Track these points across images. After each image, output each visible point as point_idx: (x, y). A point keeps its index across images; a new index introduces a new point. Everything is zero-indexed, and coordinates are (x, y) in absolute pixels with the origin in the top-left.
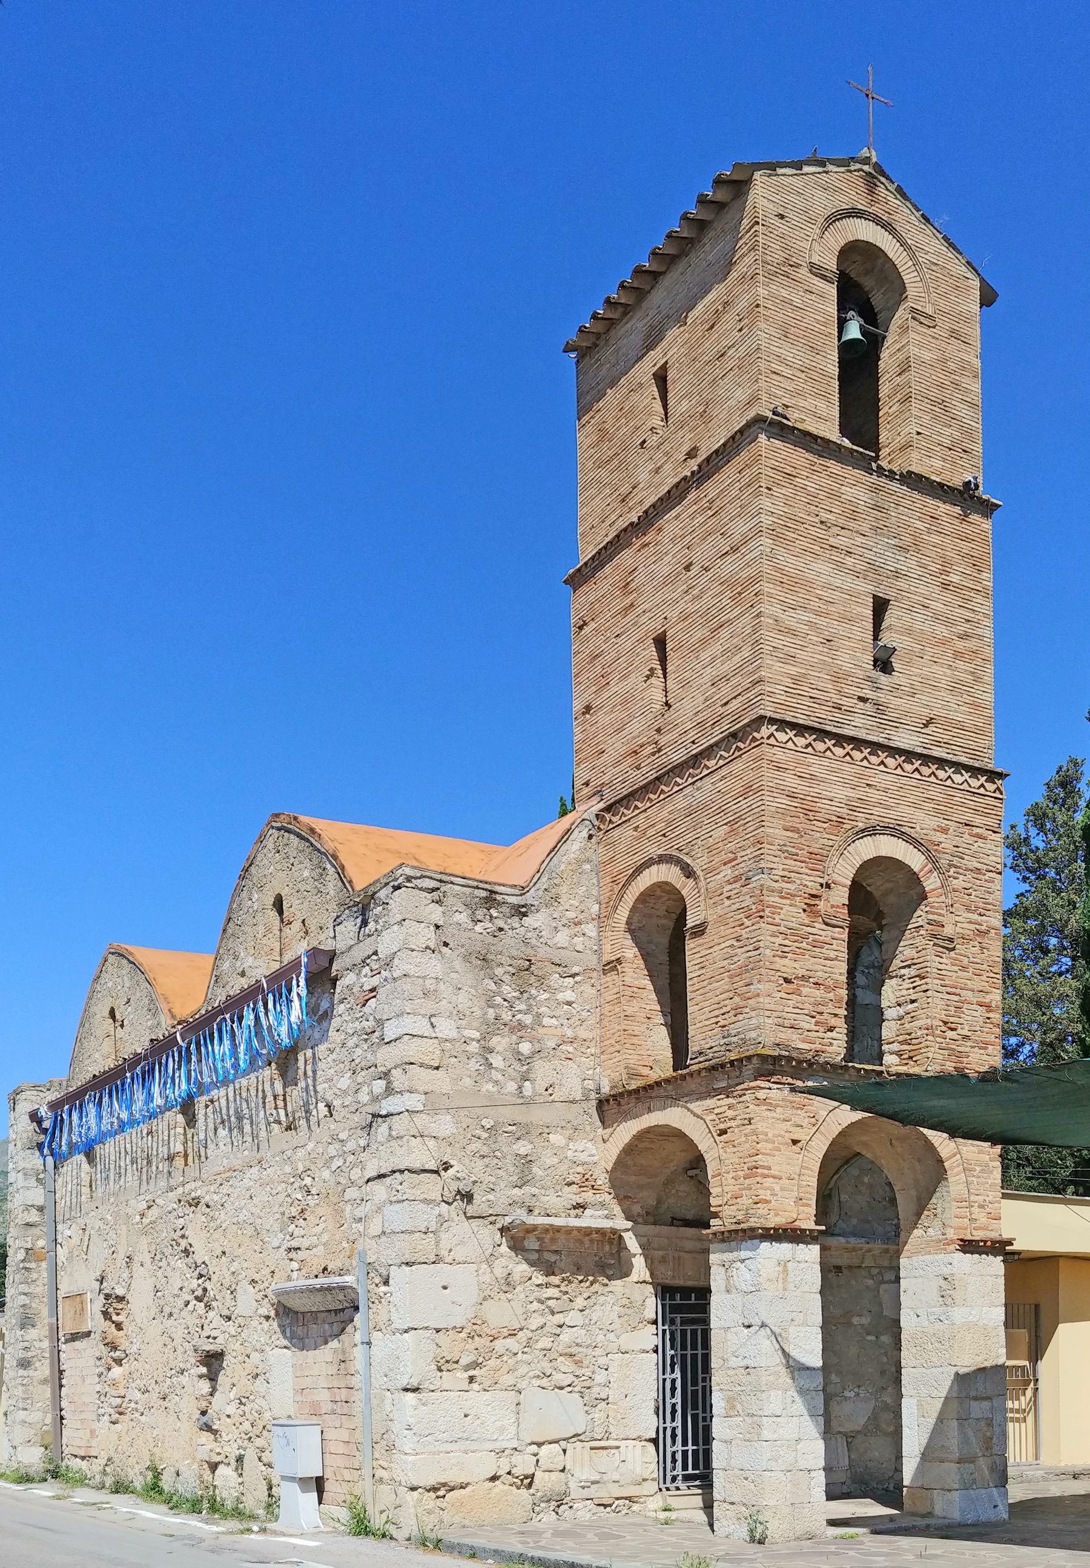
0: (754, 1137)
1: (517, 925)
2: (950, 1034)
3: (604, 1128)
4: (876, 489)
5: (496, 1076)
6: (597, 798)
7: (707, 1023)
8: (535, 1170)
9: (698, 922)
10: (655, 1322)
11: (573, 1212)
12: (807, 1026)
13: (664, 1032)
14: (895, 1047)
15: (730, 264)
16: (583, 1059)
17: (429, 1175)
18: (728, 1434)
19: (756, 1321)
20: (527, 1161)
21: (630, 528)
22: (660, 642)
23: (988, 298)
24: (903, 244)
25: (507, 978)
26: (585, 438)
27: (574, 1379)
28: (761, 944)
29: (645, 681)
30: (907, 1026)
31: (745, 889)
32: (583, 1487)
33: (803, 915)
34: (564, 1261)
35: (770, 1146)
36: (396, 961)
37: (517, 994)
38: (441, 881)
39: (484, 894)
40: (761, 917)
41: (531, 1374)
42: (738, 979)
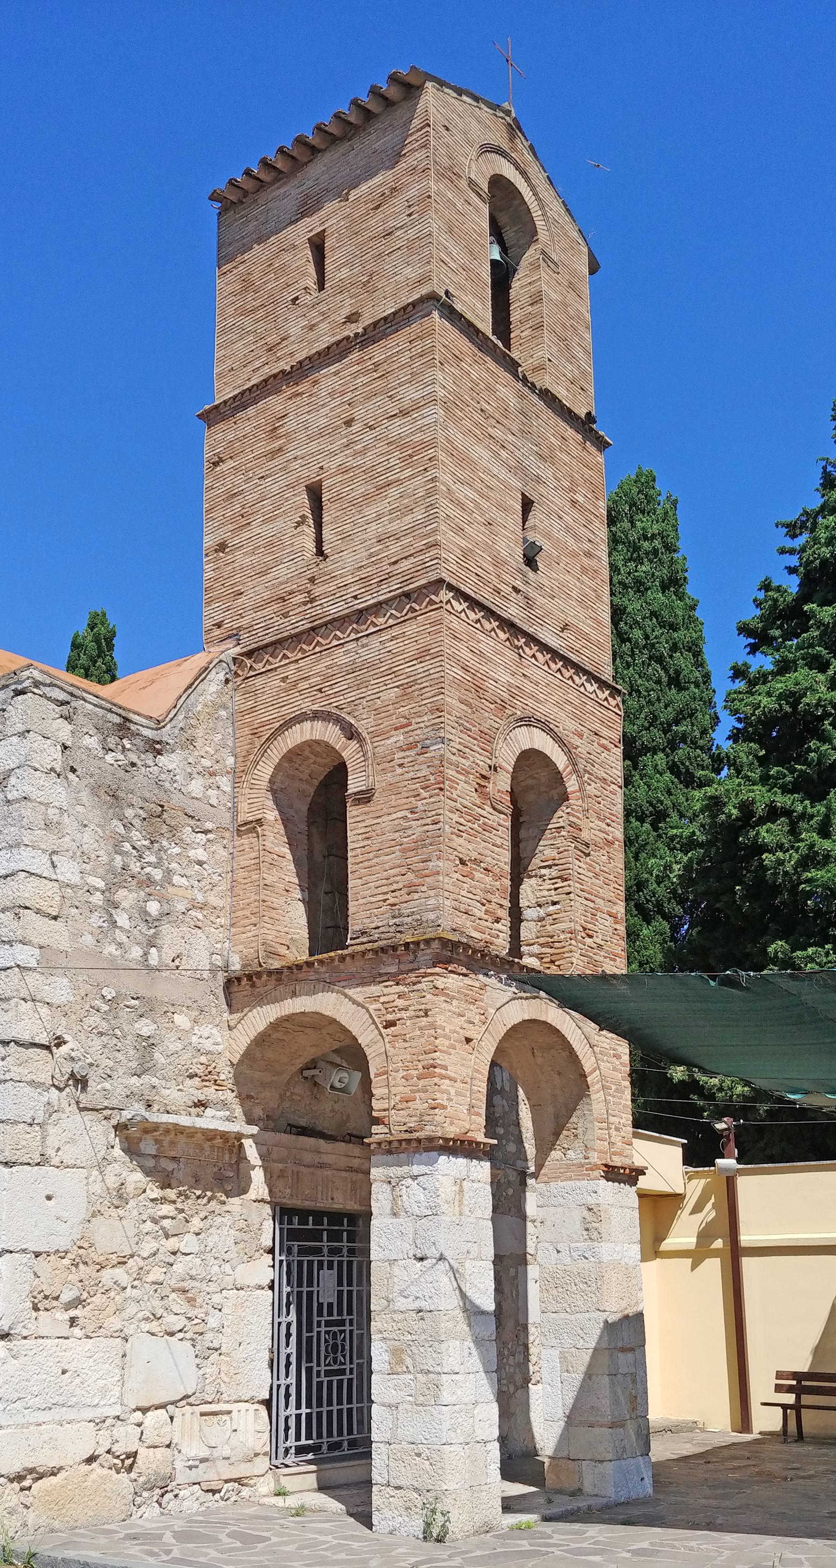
0: (432, 1032)
1: (150, 763)
2: (588, 940)
3: (231, 1013)
4: (522, 397)
5: (121, 937)
6: (230, 643)
7: (373, 899)
8: (157, 1055)
9: (364, 788)
10: (271, 1251)
11: (193, 1111)
12: (479, 914)
13: (301, 908)
14: (536, 949)
15: (398, 156)
16: (212, 930)
17: (38, 1050)
18: (392, 1396)
19: (433, 1252)
20: (148, 1044)
21: (281, 375)
22: (315, 493)
23: (594, 268)
24: (535, 194)
25: (137, 822)
26: (225, 285)
27: (186, 1322)
28: (441, 818)
29: (296, 528)
30: (549, 928)
31: (421, 758)
32: (190, 1468)
33: (474, 794)
34: (182, 1171)
35: (447, 1043)
36: (13, 780)
37: (146, 843)
38: (72, 694)
39: (117, 720)
40: (441, 789)
41: (140, 1315)
42: (412, 853)
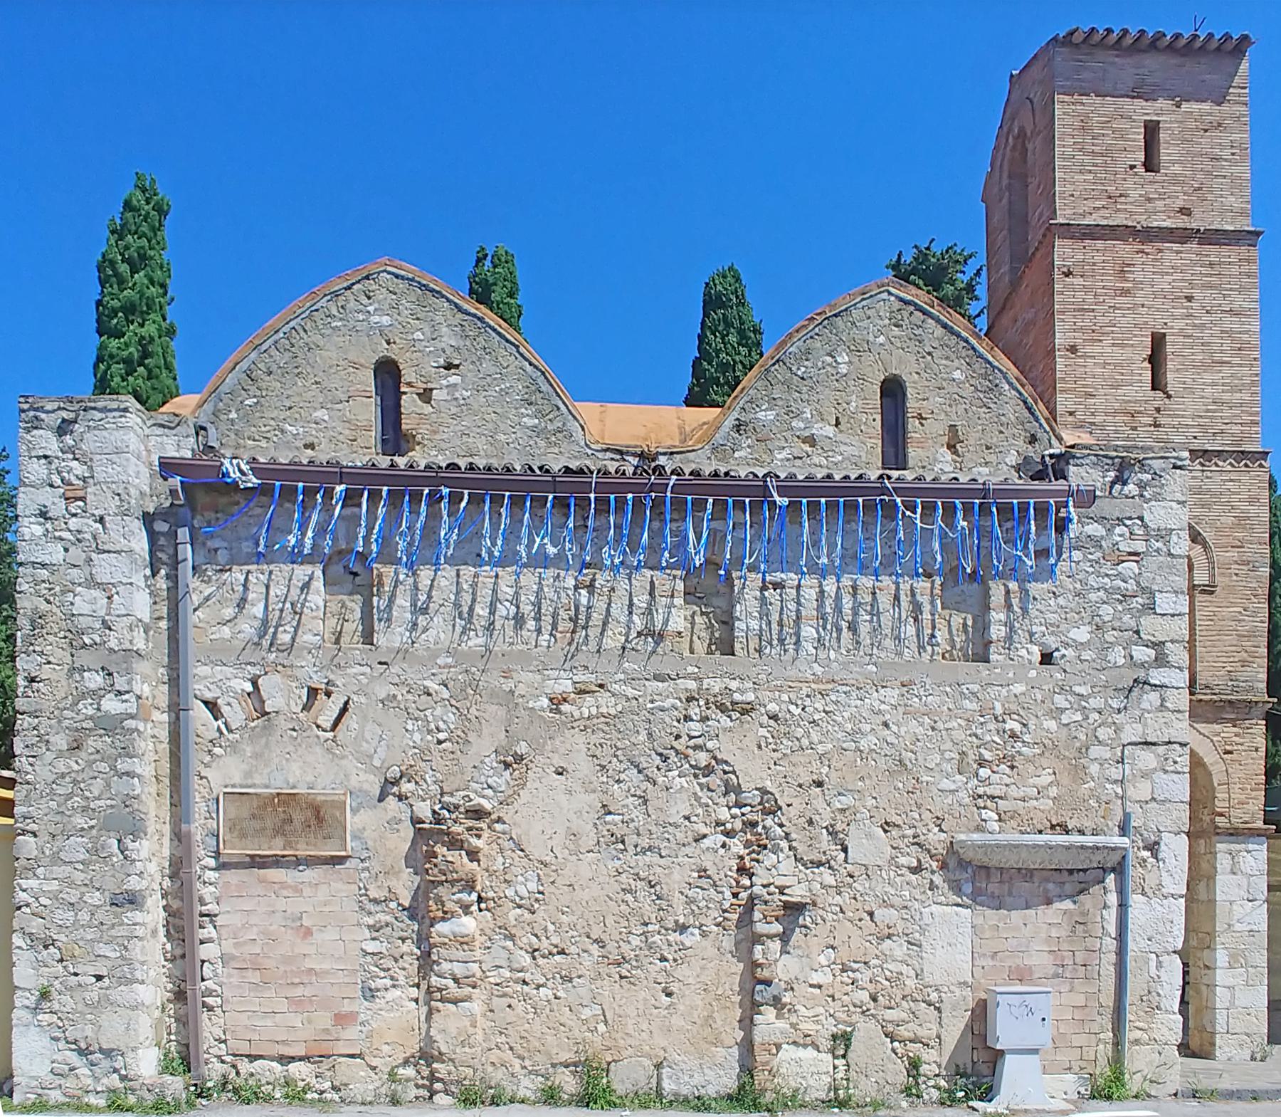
22: (1158, 342)
